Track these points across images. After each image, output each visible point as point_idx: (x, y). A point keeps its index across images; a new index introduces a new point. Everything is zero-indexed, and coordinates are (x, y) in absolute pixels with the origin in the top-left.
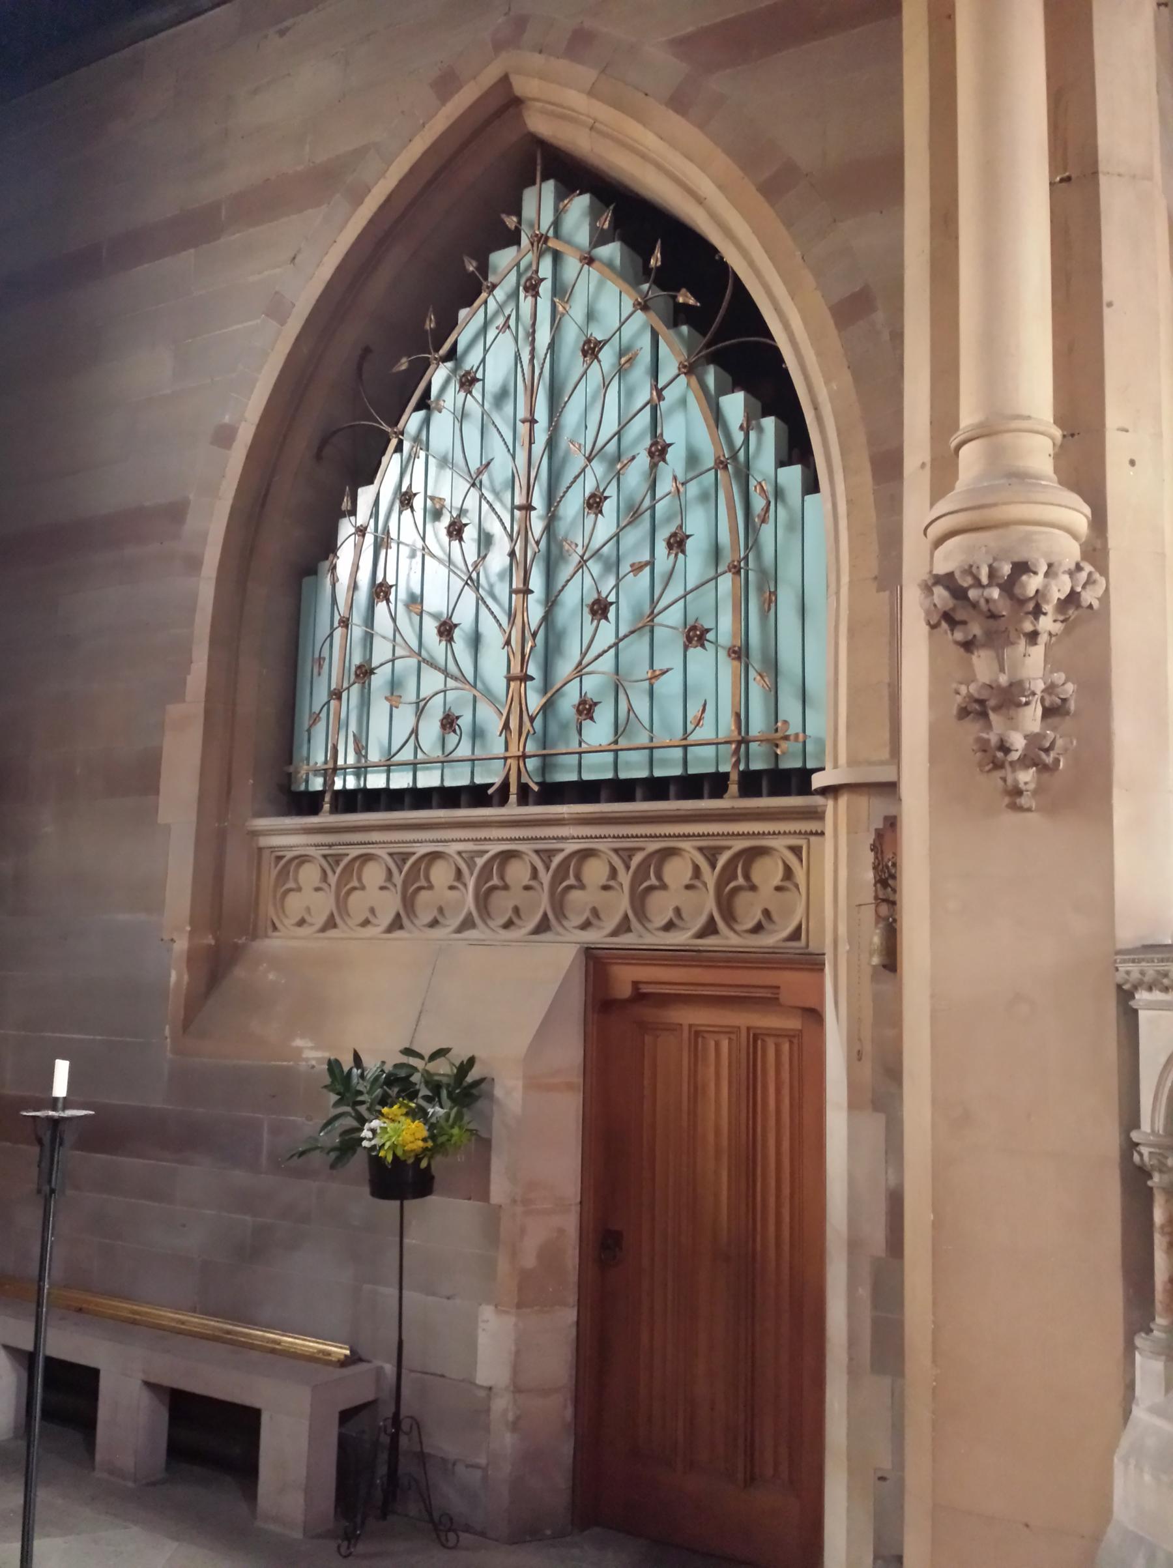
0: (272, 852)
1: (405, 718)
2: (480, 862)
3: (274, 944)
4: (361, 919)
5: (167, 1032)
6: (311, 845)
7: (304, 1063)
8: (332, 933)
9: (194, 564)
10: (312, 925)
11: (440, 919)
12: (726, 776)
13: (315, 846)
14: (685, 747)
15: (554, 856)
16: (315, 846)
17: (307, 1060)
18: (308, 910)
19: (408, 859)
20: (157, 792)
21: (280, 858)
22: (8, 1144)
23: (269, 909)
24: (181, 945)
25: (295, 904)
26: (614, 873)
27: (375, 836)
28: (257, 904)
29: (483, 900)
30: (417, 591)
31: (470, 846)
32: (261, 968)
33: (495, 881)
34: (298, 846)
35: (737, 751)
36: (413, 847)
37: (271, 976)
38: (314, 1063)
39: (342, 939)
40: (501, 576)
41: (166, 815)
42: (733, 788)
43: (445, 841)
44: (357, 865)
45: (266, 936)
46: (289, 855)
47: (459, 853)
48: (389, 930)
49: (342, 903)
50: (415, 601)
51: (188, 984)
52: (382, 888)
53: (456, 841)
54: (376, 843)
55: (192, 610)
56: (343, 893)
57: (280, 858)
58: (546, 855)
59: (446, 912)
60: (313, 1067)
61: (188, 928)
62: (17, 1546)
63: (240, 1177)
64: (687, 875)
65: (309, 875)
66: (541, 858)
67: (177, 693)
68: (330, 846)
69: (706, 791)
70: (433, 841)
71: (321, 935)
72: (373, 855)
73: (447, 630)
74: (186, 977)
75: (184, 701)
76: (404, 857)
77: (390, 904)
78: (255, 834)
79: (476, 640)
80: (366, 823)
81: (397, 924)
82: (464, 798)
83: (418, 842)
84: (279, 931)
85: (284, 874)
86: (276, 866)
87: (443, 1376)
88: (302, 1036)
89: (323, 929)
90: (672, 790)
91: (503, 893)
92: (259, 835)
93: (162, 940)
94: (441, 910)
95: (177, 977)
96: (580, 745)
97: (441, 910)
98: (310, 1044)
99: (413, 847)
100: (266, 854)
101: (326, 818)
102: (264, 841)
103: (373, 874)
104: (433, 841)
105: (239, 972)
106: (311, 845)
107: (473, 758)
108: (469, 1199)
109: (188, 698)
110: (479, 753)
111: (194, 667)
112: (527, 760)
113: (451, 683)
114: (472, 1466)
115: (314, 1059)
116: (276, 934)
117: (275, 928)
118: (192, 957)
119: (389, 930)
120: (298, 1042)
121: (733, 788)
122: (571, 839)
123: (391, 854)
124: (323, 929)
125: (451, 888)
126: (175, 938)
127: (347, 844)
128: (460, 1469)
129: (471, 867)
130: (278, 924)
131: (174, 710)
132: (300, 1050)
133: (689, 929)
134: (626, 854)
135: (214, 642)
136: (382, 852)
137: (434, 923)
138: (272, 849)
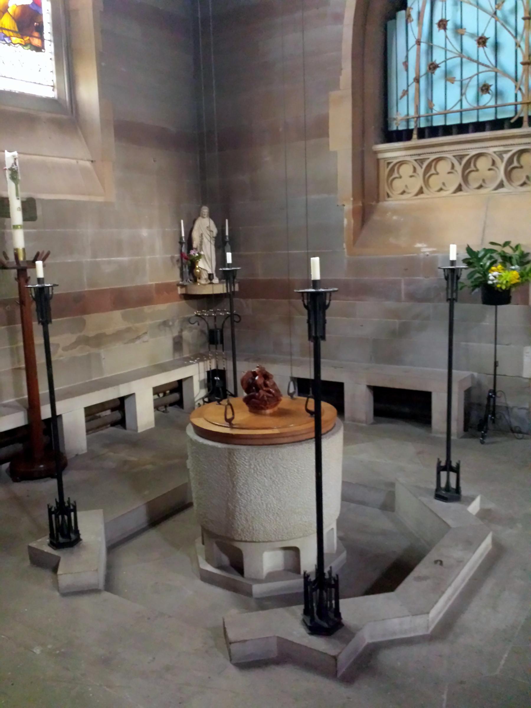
0: (385, 160)
1: (454, 90)
2: (506, 157)
3: (390, 203)
4: (438, 188)
5: (345, 245)
6: (408, 156)
7: (422, 254)
8: (421, 196)
9: (338, 18)
10: (409, 193)
11: (483, 184)
12: (412, 130)
13: (411, 155)
14: (496, 107)
15: (424, 161)
16: (411, 155)
17: (424, 252)
18: (406, 186)
19: (463, 158)
20: (327, 135)
21: (389, 164)
22: (264, 300)
23: (384, 187)
24: (349, 207)
25: (398, 185)
26: (415, 170)
27: (446, 148)
28: (378, 187)
29: (508, 174)
30: (459, 22)
31: (502, 149)
32: (388, 214)
33: (515, 164)
34: (400, 157)
35: (417, 121)
36: (468, 151)
37: (395, 218)
38: (428, 253)
39: (427, 198)
40: (511, 12)
41: (333, 146)
42: (415, 136)
43: (487, 147)
44: (433, 164)
45: (385, 201)
46: (395, 161)
47: (495, 152)
48: (456, 191)
49: (426, 182)
50: (459, 30)
51: (354, 224)
52: (449, 173)
53: (492, 147)
54: (447, 151)
55: (340, 41)
56: (389, 181)
57: (389, 164)
58: (460, 158)
59: (486, 181)
60: (428, 255)
61: (352, 199)
62: (56, 389)
63: (390, 304)
64: (448, 168)
65: (406, 170)
66: (418, 163)
67: (336, 85)
68: (419, 155)
69: (470, 130)
70: (480, 148)
71: (416, 197)
72: (485, 153)
73: (482, 41)
74: (352, 221)
75: (340, 89)
76: (461, 157)
77: (457, 179)
78: (376, 153)
79: (496, 47)
80: (441, 142)
81: (459, 189)
82: (488, 127)
83: (471, 149)
84: (391, 197)
85: (392, 171)
86: (388, 167)
87: (505, 375)
88: (420, 242)
89: (417, 195)
90: (454, 130)
91: (519, 170)
92: (378, 153)
93: (338, 205)
94: (484, 181)
95: (347, 222)
96: (432, 112)
97: (484, 181)
98: (425, 245)
99: (468, 151)
100: (382, 163)
101: (415, 141)
102: (380, 156)
103: (443, 167)
104: (480, 148)
105: (376, 217)
106: (408, 156)
107: (478, 108)
108: (518, 304)
109: (341, 87)
110: (499, 102)
111: (343, 72)
112: (443, 116)
113: (482, 68)
114: (522, 408)
115: (429, 252)
116: (390, 199)
117: (388, 196)
118: (354, 212)
119: (456, 191)
120: (418, 245)
121: (415, 136)
122: (472, 150)
123: (454, 156)
124: (417, 195)
125: (490, 170)
126: (345, 204)
127: (429, 153)
128: (515, 410)
129: (502, 159)
130: (390, 194)
131: (334, 94)
132: (419, 249)
133: (489, 187)
134: (500, 155)
135: (354, 57)
136: (449, 156)
137: (480, 187)
138: (385, 159)
